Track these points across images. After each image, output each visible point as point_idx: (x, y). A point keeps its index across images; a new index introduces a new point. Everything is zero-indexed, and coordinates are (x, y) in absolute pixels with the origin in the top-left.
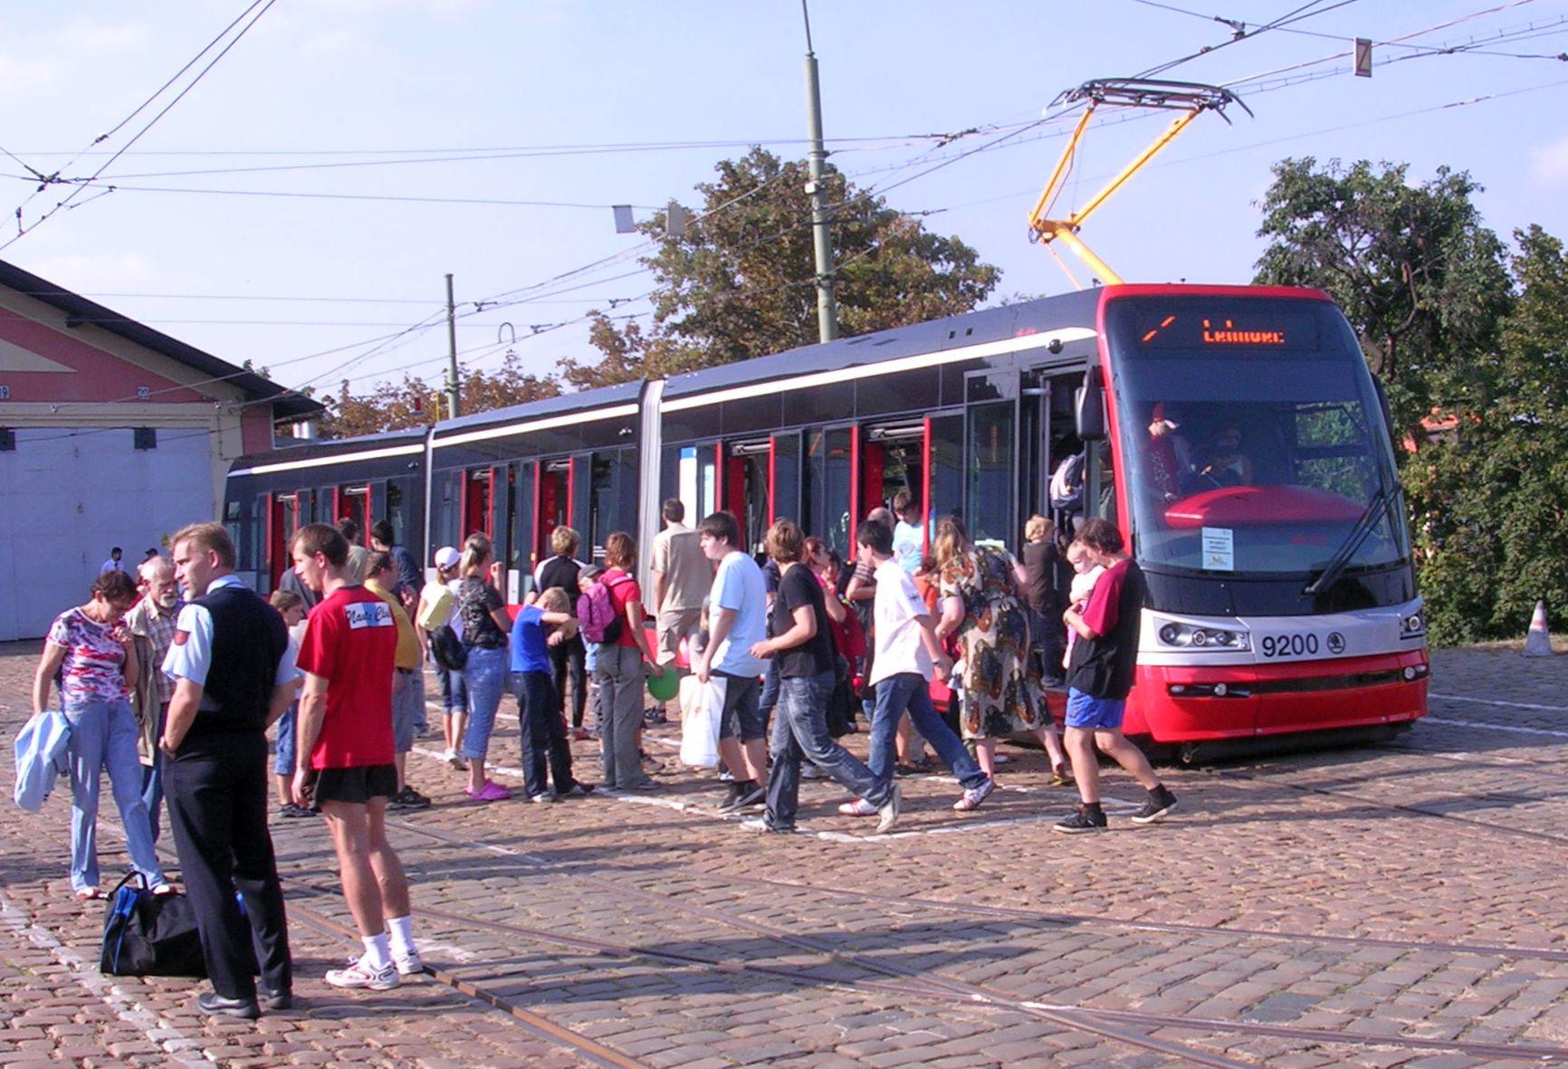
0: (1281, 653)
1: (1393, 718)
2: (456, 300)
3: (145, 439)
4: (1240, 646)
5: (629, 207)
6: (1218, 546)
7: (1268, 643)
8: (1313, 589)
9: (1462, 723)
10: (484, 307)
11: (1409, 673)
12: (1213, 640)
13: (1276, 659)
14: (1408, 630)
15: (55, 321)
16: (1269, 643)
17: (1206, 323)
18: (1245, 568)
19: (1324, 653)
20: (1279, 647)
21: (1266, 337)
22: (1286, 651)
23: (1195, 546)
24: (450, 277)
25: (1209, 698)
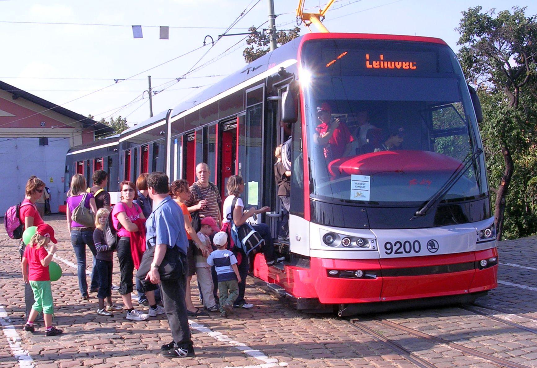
0: (396, 252)
1: (473, 290)
2: (152, 87)
3: (44, 142)
4: (370, 248)
5: (141, 26)
6: (361, 185)
7: (388, 247)
8: (420, 212)
9: (524, 287)
10: (118, 81)
11: (484, 263)
12: (354, 244)
13: (393, 255)
14: (483, 237)
15: (8, 98)
16: (389, 246)
17: (367, 56)
18: (380, 199)
19: (425, 252)
20: (395, 248)
21: (405, 65)
22: (399, 251)
23: (347, 186)
24: (150, 77)
25: (353, 279)
